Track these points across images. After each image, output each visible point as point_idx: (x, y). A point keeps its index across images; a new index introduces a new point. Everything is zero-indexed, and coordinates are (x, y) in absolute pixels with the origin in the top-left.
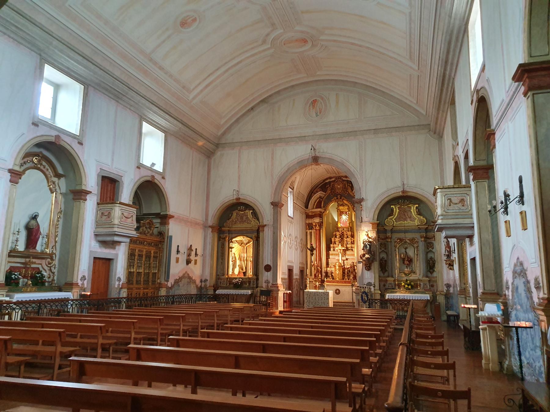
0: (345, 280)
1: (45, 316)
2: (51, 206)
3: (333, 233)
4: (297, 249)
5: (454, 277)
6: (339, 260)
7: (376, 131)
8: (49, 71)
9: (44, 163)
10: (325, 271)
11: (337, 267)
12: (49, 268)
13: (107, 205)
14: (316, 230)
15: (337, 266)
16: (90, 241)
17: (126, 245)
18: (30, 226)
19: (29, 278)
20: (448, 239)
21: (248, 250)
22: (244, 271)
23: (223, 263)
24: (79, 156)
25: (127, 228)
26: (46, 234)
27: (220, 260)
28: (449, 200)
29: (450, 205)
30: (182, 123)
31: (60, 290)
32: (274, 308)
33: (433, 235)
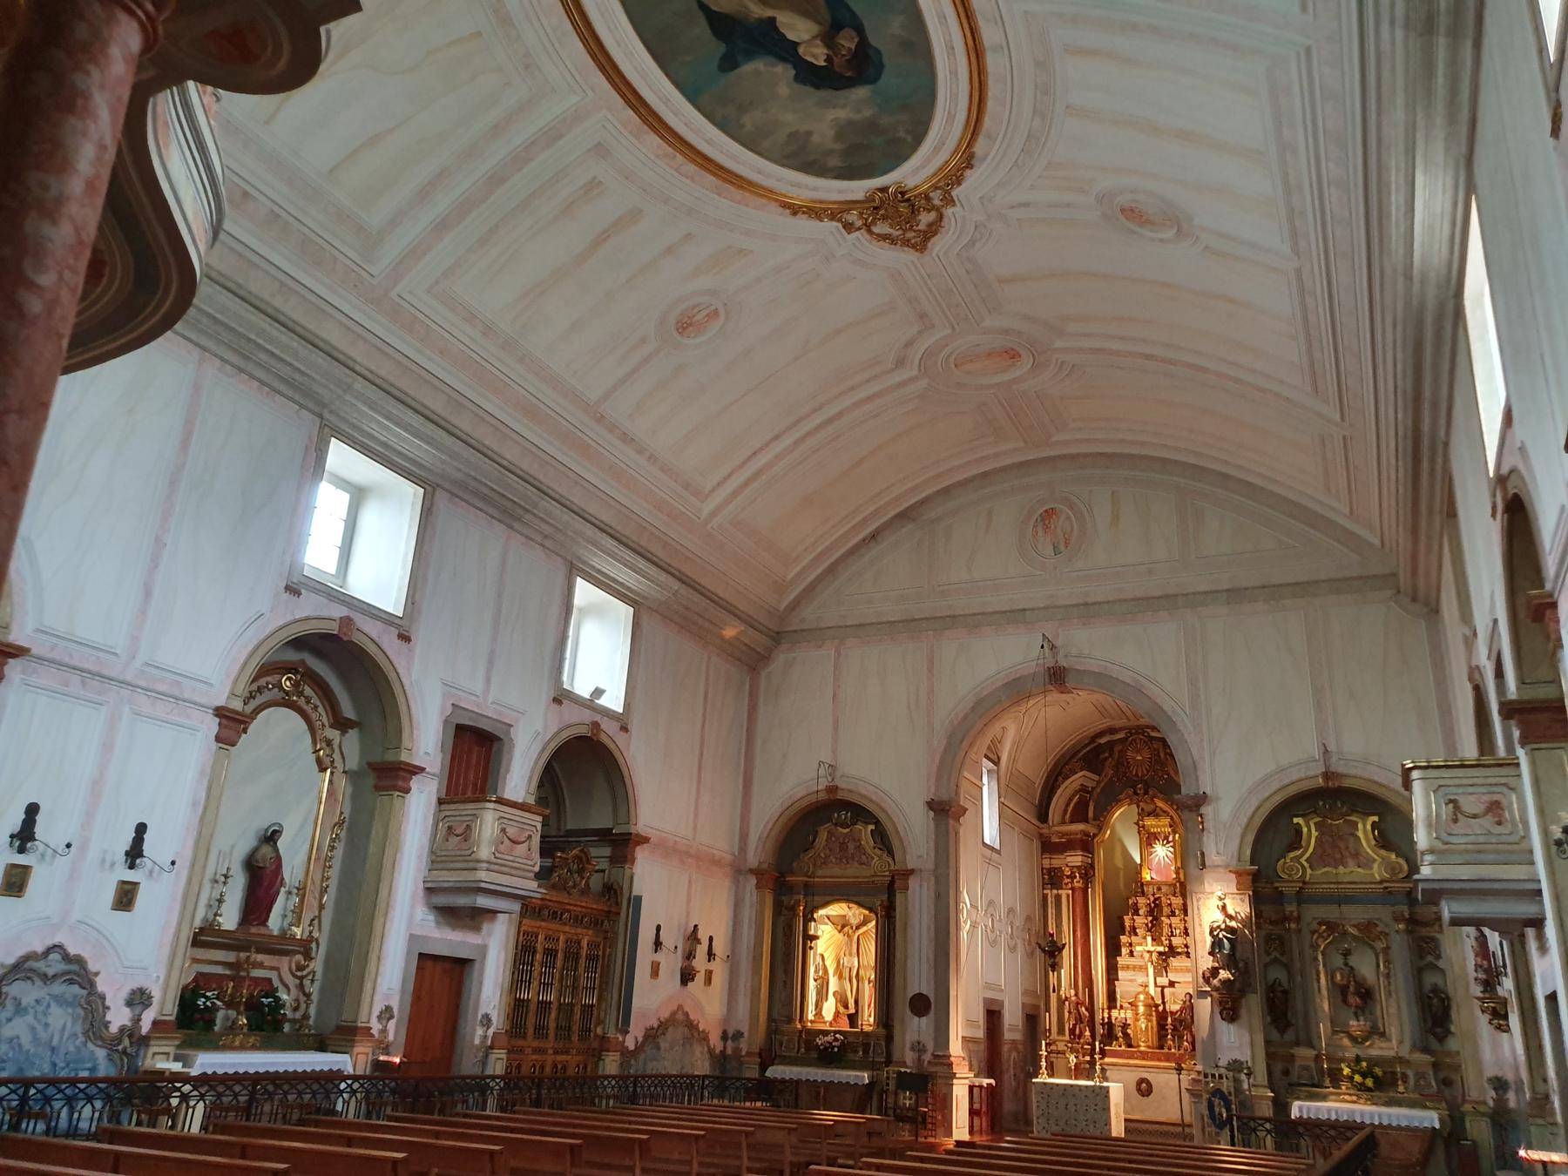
0: (1166, 1050)
1: (264, 1124)
2: (316, 808)
3: (1128, 899)
4: (1013, 949)
5: (1515, 1059)
6: (1146, 986)
7: (1236, 595)
8: (340, 456)
9: (308, 691)
10: (1103, 1019)
11: (1141, 1009)
12: (298, 981)
13: (461, 806)
14: (1073, 889)
15: (1140, 1004)
16: (412, 907)
17: (510, 920)
18: (257, 861)
19: (242, 1008)
20: (1483, 928)
21: (862, 947)
22: (852, 1011)
23: (788, 984)
24: (399, 671)
25: (513, 872)
26: (297, 885)
27: (780, 976)
28: (1451, 806)
29: (1456, 821)
30: (680, 580)
31: (322, 1047)
32: (940, 1131)
33: (1436, 913)
